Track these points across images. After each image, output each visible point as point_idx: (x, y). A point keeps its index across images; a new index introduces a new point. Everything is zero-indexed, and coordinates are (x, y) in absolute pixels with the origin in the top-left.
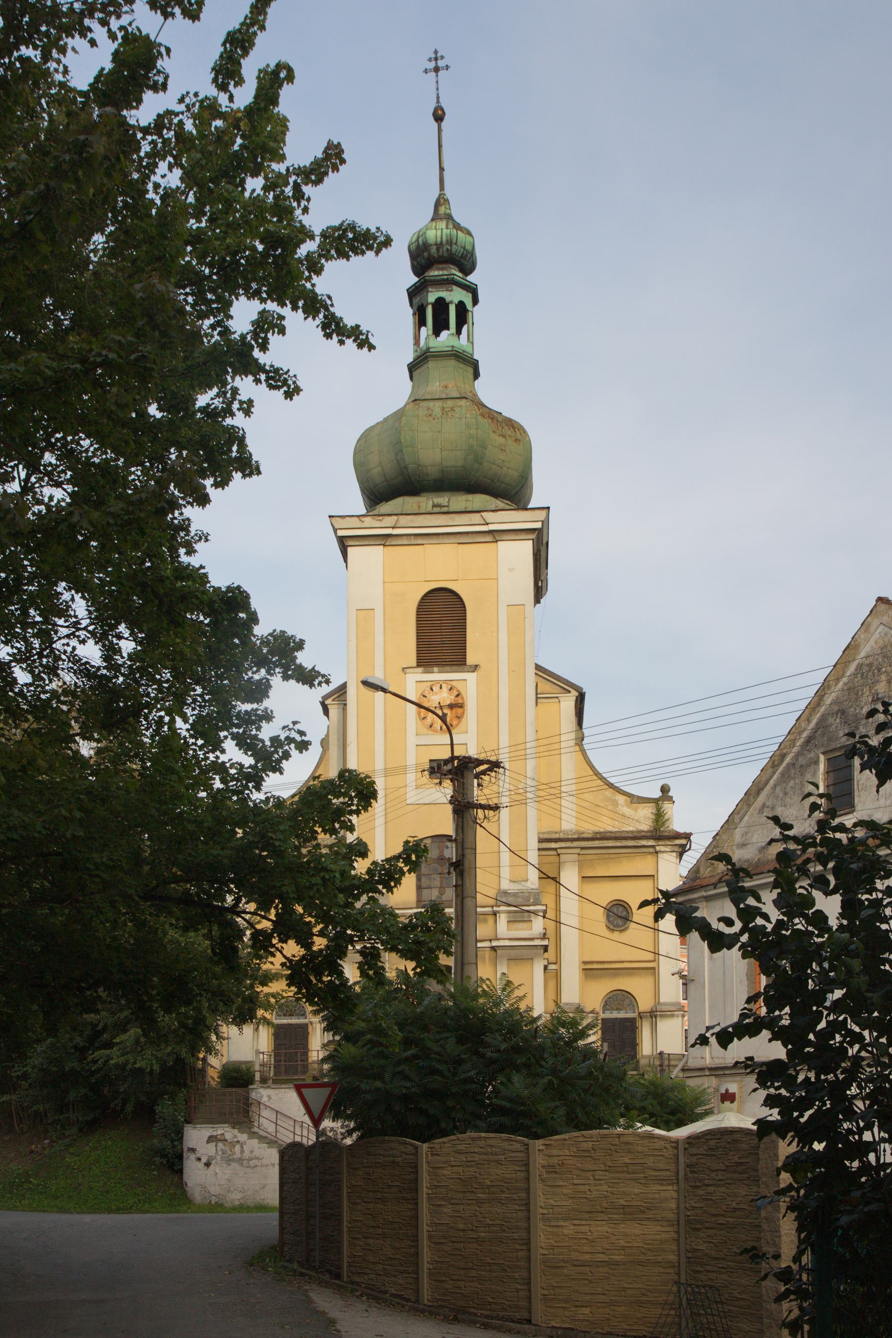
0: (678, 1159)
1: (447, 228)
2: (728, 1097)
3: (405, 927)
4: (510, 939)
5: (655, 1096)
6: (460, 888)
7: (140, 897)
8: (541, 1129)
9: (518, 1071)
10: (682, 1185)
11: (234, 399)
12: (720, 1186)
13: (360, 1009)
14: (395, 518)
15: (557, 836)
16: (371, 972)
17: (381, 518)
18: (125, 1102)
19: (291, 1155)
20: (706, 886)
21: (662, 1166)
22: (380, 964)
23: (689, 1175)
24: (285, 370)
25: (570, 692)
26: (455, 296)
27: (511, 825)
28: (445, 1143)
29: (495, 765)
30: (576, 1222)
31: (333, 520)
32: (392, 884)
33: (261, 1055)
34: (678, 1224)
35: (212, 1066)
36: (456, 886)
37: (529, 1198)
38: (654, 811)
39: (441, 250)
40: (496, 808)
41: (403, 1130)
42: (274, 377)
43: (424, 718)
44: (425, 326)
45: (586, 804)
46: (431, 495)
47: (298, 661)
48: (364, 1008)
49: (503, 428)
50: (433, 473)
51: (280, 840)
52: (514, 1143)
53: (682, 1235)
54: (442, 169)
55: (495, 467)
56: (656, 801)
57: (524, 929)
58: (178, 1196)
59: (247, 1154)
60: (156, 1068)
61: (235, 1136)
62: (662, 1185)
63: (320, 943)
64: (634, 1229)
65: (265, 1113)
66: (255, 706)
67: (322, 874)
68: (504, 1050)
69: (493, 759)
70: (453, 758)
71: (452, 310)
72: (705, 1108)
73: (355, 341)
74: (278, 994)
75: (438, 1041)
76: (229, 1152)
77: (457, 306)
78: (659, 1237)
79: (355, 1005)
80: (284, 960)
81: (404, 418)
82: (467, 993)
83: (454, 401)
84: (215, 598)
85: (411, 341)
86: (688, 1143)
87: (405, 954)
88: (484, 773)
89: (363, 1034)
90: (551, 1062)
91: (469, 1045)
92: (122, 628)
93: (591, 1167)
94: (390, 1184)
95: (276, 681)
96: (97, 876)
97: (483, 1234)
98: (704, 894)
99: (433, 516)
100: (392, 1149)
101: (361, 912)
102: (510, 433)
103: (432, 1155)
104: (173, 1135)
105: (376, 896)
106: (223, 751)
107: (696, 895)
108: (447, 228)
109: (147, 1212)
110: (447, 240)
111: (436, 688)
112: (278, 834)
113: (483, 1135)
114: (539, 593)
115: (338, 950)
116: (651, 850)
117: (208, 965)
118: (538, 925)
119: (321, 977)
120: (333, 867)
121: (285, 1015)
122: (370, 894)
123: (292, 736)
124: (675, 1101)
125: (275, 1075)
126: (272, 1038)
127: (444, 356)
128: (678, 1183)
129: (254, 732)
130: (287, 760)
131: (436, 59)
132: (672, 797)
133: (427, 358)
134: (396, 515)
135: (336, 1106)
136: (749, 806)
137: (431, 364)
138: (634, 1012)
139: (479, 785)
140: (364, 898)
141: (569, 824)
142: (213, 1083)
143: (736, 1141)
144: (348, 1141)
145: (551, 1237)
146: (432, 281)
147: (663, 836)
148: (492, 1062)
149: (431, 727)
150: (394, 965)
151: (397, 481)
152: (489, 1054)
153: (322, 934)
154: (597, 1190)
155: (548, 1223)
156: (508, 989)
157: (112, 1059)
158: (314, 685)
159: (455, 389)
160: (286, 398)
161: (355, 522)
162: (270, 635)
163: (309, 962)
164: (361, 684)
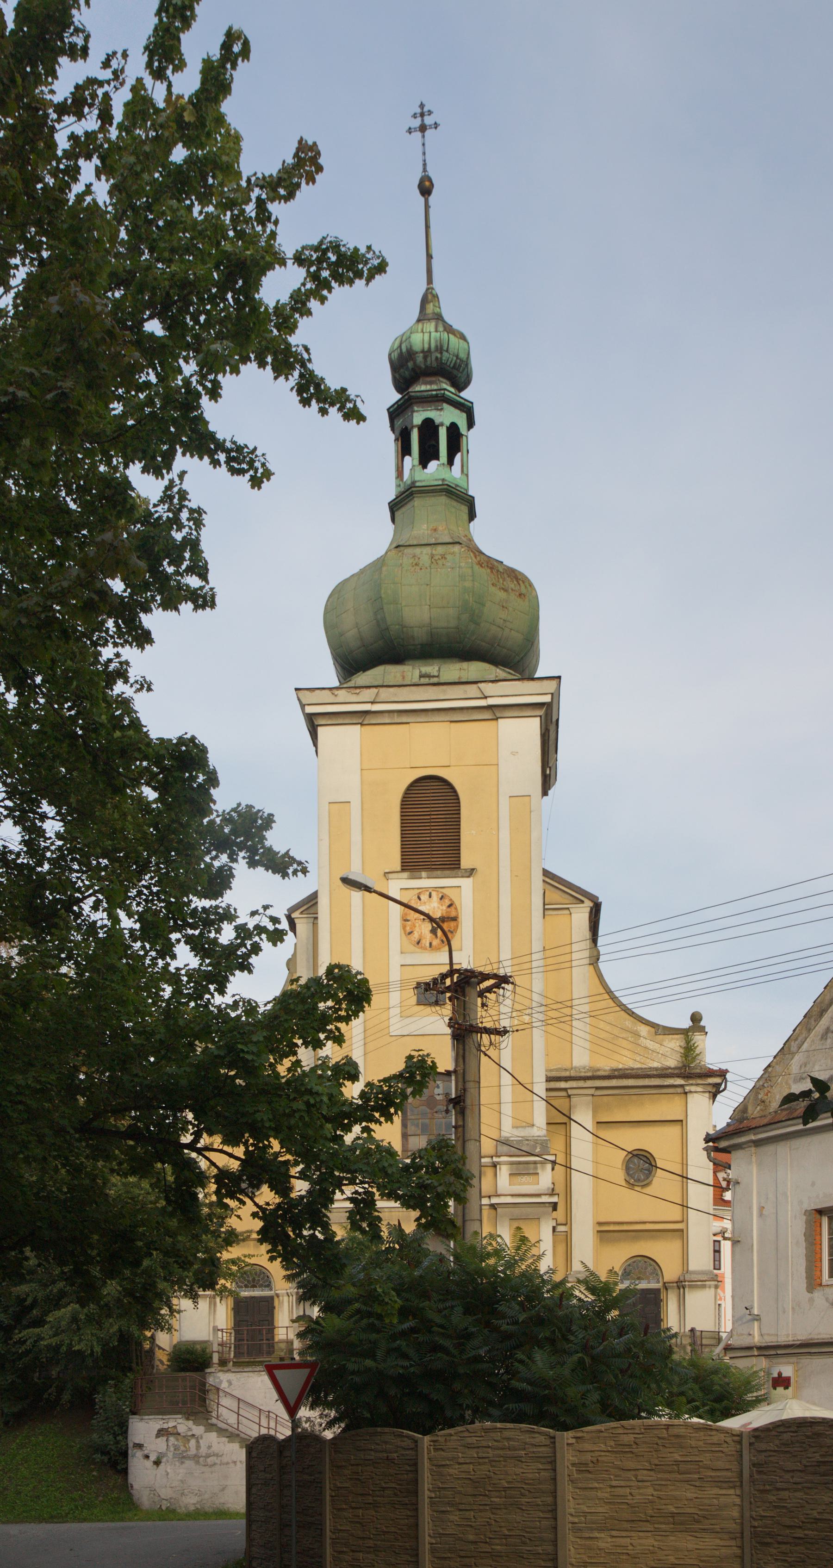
0: (741, 1456)
1: (436, 331)
2: (782, 1382)
3: (407, 1167)
4: (512, 1195)
5: (696, 1380)
6: (460, 1130)
7: (74, 1129)
8: (572, 1419)
9: (541, 1347)
10: (746, 1488)
11: (182, 507)
12: (796, 1490)
13: (349, 1270)
14: (375, 690)
15: (567, 1074)
16: (364, 1225)
17: (358, 691)
18: (60, 1390)
19: (261, 1451)
20: (756, 1128)
21: (720, 1464)
22: (376, 1214)
23: (756, 1476)
24: (251, 448)
25: (582, 902)
26: (446, 416)
28: (451, 1435)
29: (503, 980)
30: (614, 1533)
31: (301, 693)
32: (392, 1110)
33: (220, 1333)
34: (742, 1537)
35: (160, 1348)
36: (456, 1127)
37: (555, 1504)
38: (683, 1044)
39: (429, 359)
40: (502, 1032)
41: (399, 1419)
42: (238, 458)
43: (410, 933)
44: (410, 454)
45: (603, 1035)
46: (418, 663)
47: (267, 844)
48: (354, 1270)
49: (504, 580)
50: (420, 635)
51: (253, 1053)
52: (535, 1436)
53: (747, 1550)
54: (429, 257)
55: (494, 628)
56: (685, 1032)
57: (529, 1184)
58: (121, 1500)
59: (203, 1450)
60: (98, 1349)
61: (190, 1429)
62: (721, 1488)
63: (301, 1187)
64: (686, 1542)
65: (225, 1401)
66: (213, 903)
67: (305, 1098)
68: (523, 1322)
69: (502, 972)
70: (451, 972)
71: (443, 434)
72: (755, 1394)
73: (340, 410)
74: (239, 1259)
75: (440, 1311)
76: (182, 1448)
77: (448, 429)
78: (717, 1553)
79: (344, 1266)
80: (256, 1209)
81: (384, 569)
82: (472, 1254)
83: (445, 547)
84: (162, 752)
85: (393, 473)
86: (756, 1437)
87: (408, 1203)
88: (489, 990)
89: (350, 1302)
90: (581, 1336)
91: (480, 1316)
92: (46, 807)
93: (631, 1465)
94: (384, 1485)
95: (241, 868)
96: (21, 1102)
97: (499, 1547)
98: (753, 1138)
99: (420, 688)
100: (386, 1443)
101: (353, 1148)
102: (513, 586)
103: (436, 1450)
104: (116, 1428)
105: (373, 1126)
106: (174, 957)
107: (743, 1139)
108: (436, 331)
109: (85, 1520)
110: (436, 346)
112: (249, 1045)
113: (499, 1425)
114: (547, 782)
115: (321, 1197)
116: (679, 1090)
117: (160, 1218)
118: (546, 1178)
119: (301, 1231)
120: (319, 1089)
121: (246, 1286)
122: (364, 1124)
123: (262, 924)
124: (720, 1385)
125: (235, 1357)
126: (231, 1314)
127: (433, 491)
128: (741, 1486)
129: (212, 935)
130: (257, 954)
131: (422, 115)
132: (704, 1027)
133: (412, 494)
134: (376, 687)
135: (315, 1392)
136: (809, 1030)
137: (417, 502)
138: (658, 1282)
139: (483, 1005)
140: (357, 1129)
141: (581, 1058)
142: (162, 1368)
143: (818, 1435)
144: (329, 1435)
145: (583, 1551)
146: (418, 398)
147: (696, 1074)
148: (507, 1336)
149: (418, 943)
150: (393, 1214)
151: (378, 645)
152: (504, 1327)
153: (303, 1176)
154: (641, 1494)
155: (578, 1534)
156: (524, 1248)
157: (43, 1339)
158: (287, 875)
159: (446, 532)
160: (253, 487)
161: (326, 696)
162: (234, 810)
163: (286, 1212)
164: (340, 882)
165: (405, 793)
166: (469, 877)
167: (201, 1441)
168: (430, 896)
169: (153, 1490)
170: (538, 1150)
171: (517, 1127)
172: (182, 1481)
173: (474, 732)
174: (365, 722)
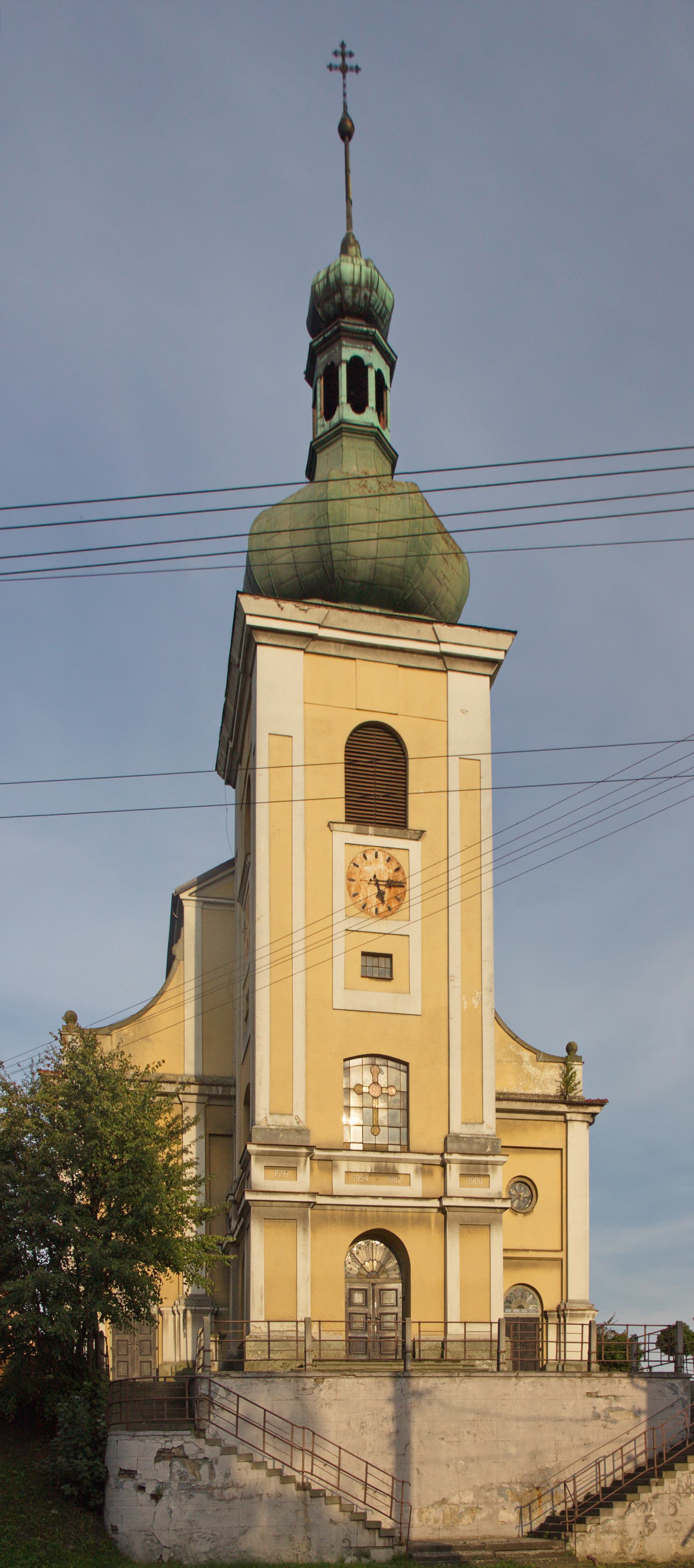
43: (355, 895)
50: (363, 570)
57: (479, 1186)
61: (201, 1450)
76: (191, 1477)
104: (88, 1449)
110: (367, 282)
111: (370, 856)
116: (561, 1118)
127: (362, 433)
133: (340, 432)
149: (364, 907)
165: (351, 735)
166: (417, 840)
167: (215, 1467)
168: (376, 856)
169: (150, 1535)
170: (489, 1149)
171: (466, 1124)
172: (189, 1521)
173: (424, 682)
174: (309, 650)
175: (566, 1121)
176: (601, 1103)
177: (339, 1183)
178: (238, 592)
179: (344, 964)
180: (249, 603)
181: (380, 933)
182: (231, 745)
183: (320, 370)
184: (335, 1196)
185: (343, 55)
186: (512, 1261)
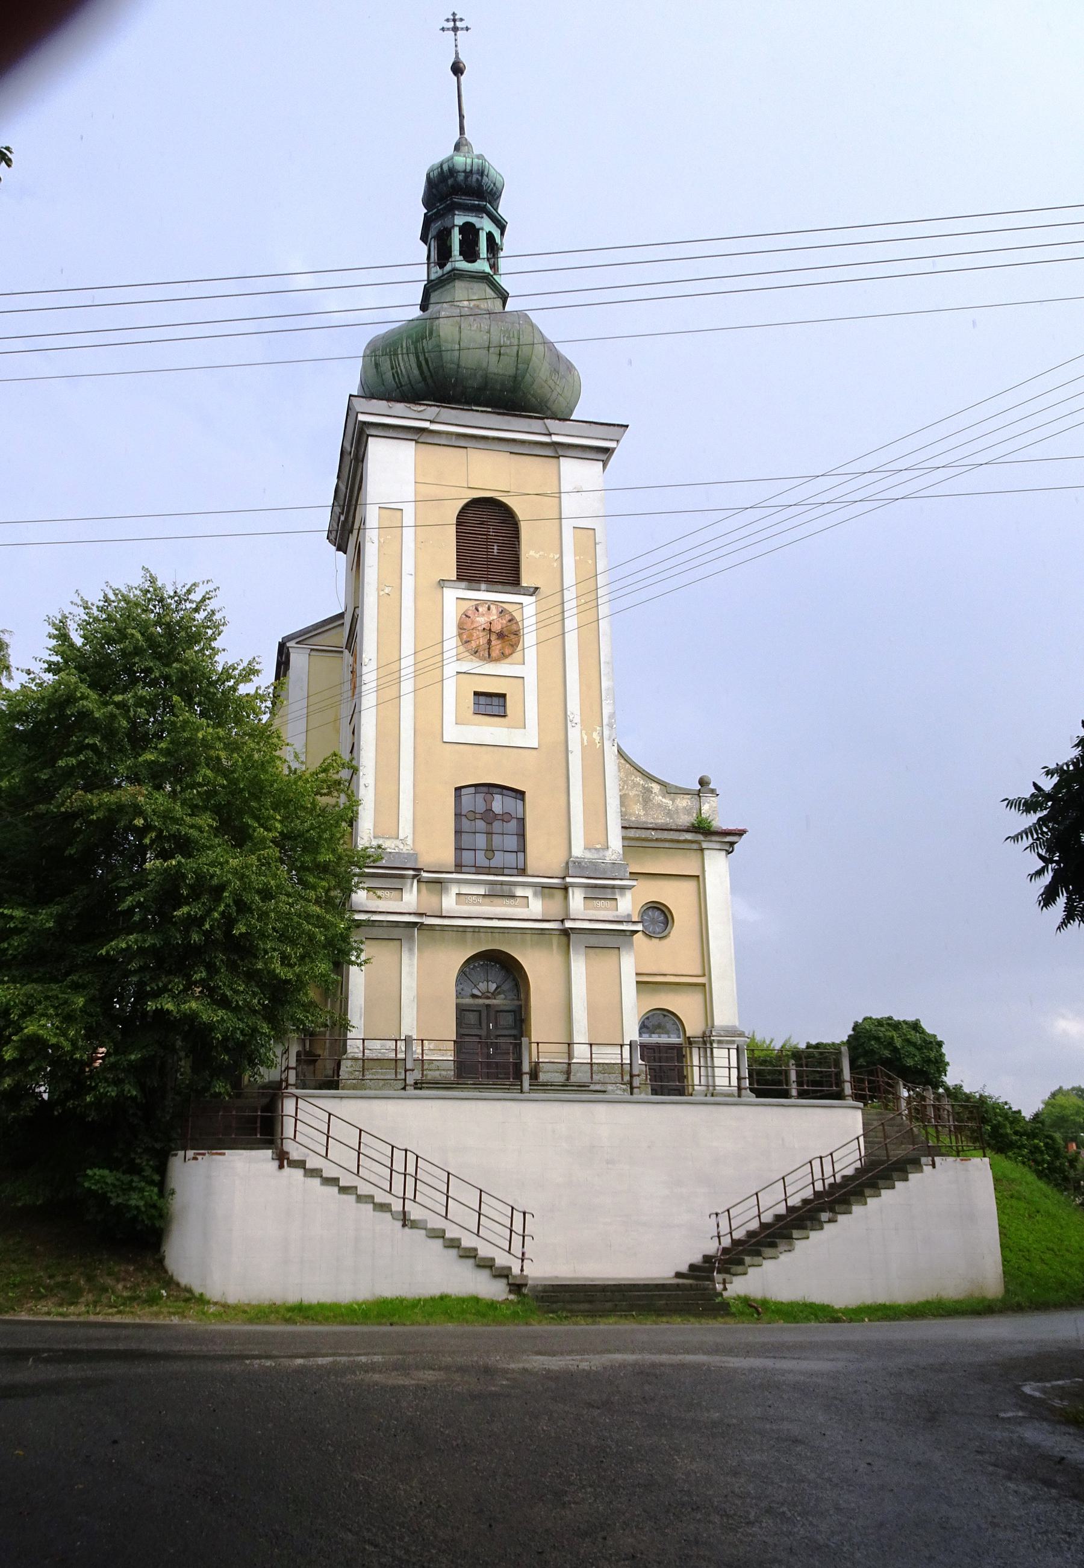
27: (584, 779)
43: (467, 642)
54: (461, 117)
57: (606, 909)
116: (695, 846)
131: (454, 20)
168: (489, 609)
175: (702, 850)
176: (740, 833)
177: (449, 902)
178: (351, 396)
179: (454, 696)
180: (360, 404)
181: (494, 675)
182: (342, 518)
183: (432, 232)
184: (445, 917)
185: (454, 20)
186: (644, 985)
